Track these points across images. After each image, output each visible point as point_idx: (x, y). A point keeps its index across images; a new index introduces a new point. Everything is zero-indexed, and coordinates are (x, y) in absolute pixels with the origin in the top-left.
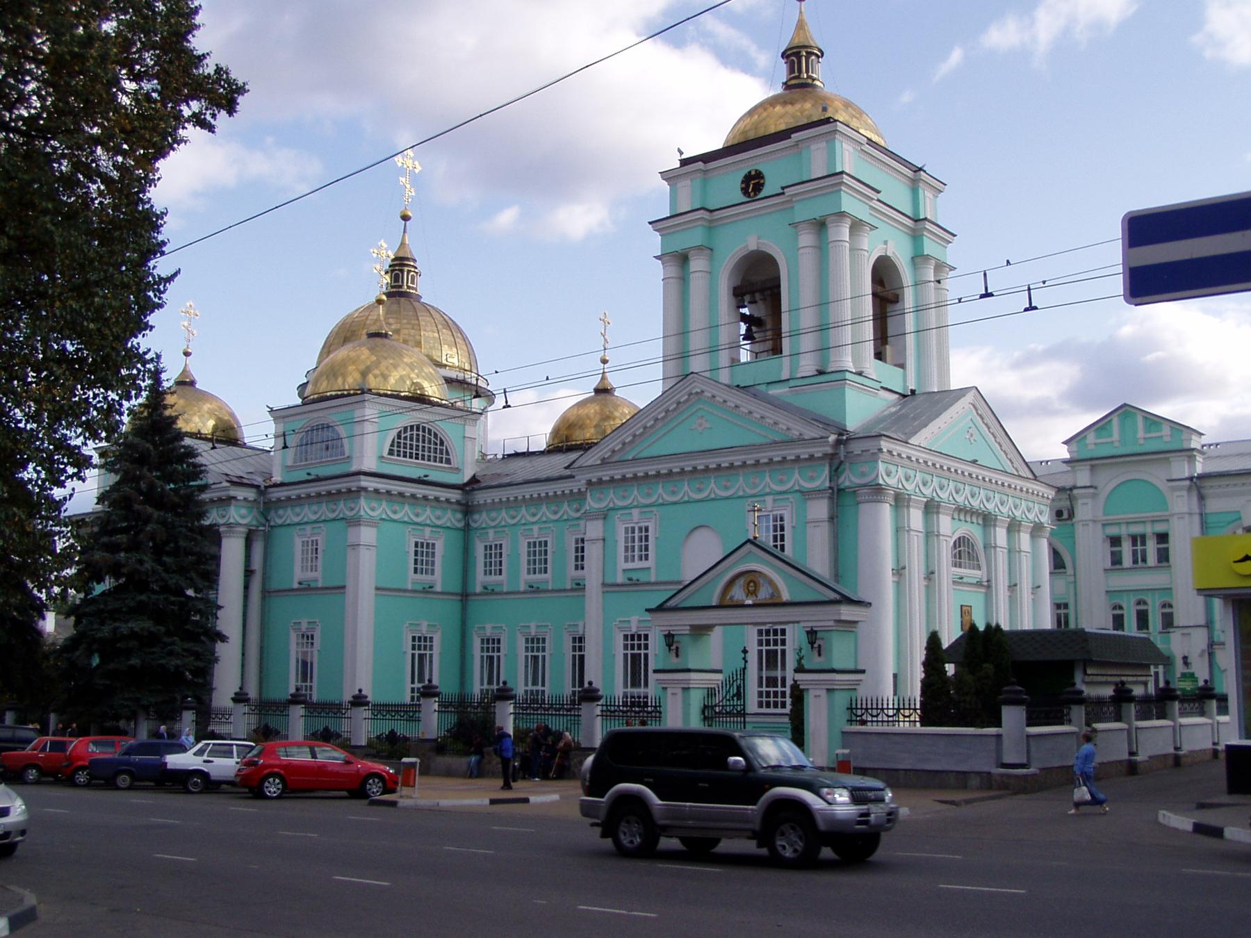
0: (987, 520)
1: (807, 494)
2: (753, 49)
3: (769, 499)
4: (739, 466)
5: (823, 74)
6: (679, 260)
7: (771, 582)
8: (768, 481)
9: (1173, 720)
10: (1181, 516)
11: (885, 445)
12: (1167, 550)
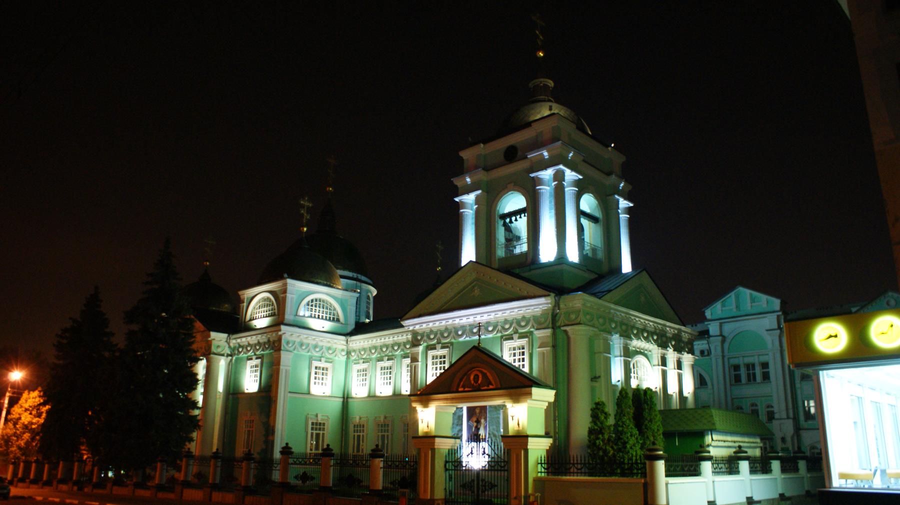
12: (768, 373)
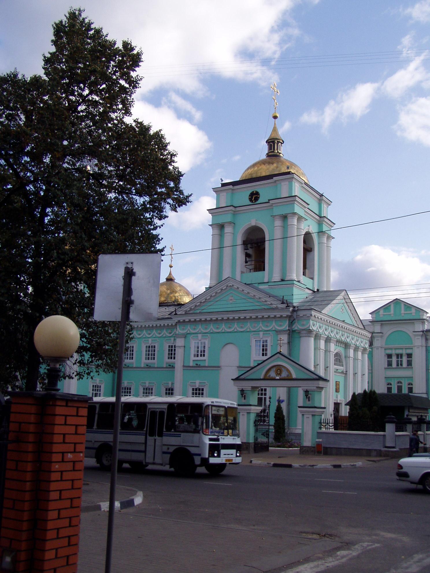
0: (347, 346)
1: (278, 332)
2: (193, 111)
3: (261, 333)
4: (249, 319)
5: (284, 151)
6: (219, 227)
7: (288, 370)
8: (261, 325)
9: (424, 432)
10: (418, 347)
11: (313, 313)
